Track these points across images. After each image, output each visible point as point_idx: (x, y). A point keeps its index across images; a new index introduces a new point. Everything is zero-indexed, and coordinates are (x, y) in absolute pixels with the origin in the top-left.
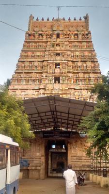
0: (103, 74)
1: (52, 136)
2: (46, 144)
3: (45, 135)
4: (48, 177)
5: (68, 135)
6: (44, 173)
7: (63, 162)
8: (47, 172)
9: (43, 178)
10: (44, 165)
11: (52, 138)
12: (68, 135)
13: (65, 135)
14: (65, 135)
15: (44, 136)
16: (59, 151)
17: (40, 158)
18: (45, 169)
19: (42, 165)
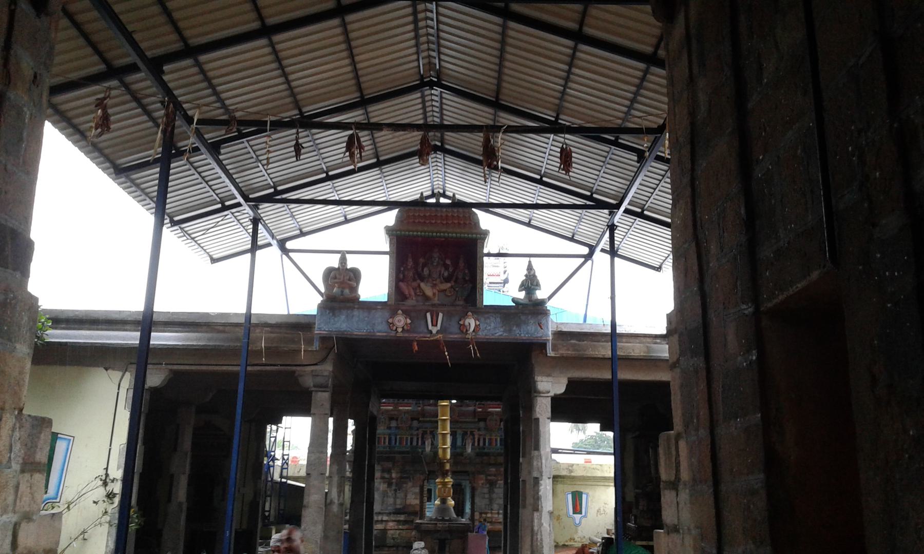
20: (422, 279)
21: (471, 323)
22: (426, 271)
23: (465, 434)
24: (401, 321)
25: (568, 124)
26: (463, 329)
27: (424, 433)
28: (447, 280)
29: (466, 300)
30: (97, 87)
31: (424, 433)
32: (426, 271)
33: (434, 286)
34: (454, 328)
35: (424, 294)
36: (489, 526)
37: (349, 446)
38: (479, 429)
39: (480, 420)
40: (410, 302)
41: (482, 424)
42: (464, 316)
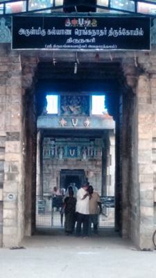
0: (38, 121)
1: (61, 40)
2: (30, 76)
3: (22, 31)
4: (37, 233)
5: (139, 32)
6: (21, 217)
7: (82, 171)
8: (30, 215)
9: (17, 240)
10: (19, 178)
11: (56, 48)
12: (139, 32)
13: (123, 32)
14: (123, 32)
15: (19, 41)
16: (76, 124)
17: (67, 266)
18: (25, 197)
19: (11, 178)
20: (70, 104)
21: (88, 122)
22: (71, 102)
23: (82, 148)
24: (63, 122)
25: (120, 13)
26: (85, 125)
27: (59, 148)
28: (79, 105)
29: (86, 113)
30: (92, 253)
31: (59, 148)
32: (71, 102)
33: (74, 107)
34: (81, 123)
35: (70, 111)
36: (11, 172)
37: (76, 226)
38: (90, 146)
39: (91, 140)
40: (67, 113)
41: (92, 143)
42: (85, 120)
